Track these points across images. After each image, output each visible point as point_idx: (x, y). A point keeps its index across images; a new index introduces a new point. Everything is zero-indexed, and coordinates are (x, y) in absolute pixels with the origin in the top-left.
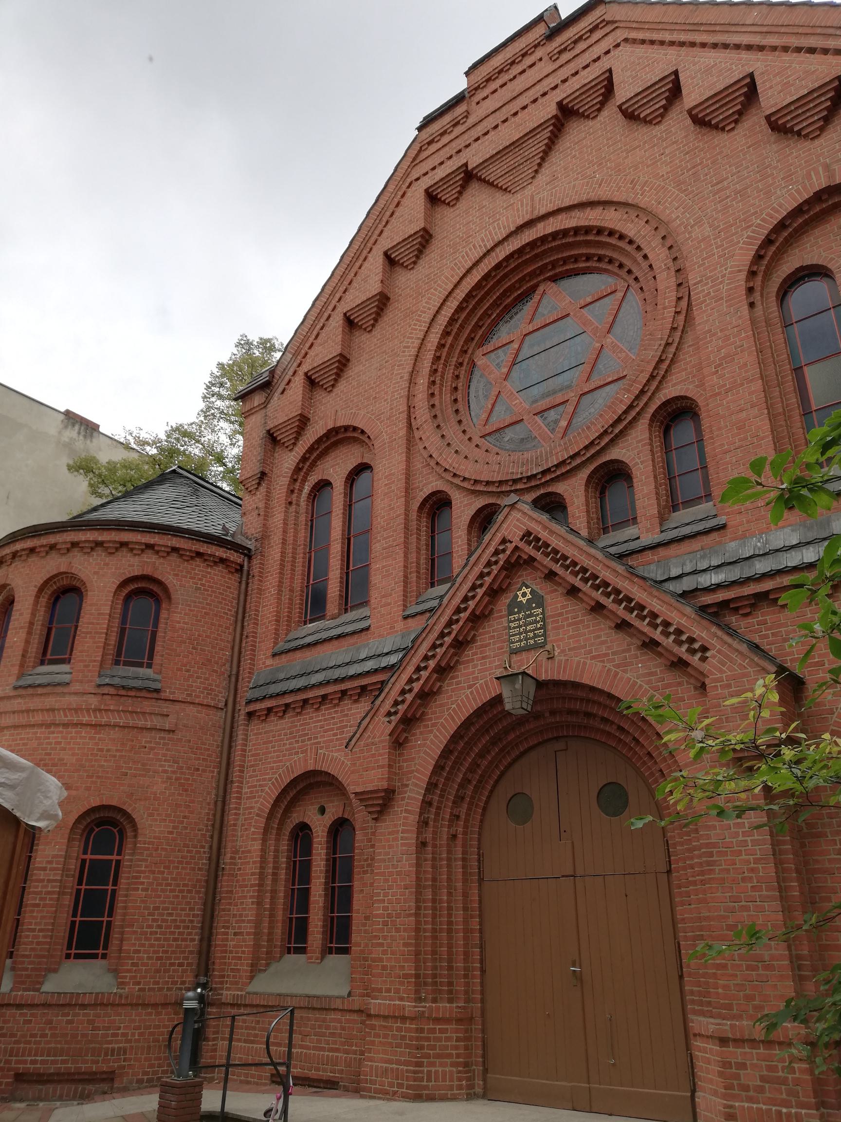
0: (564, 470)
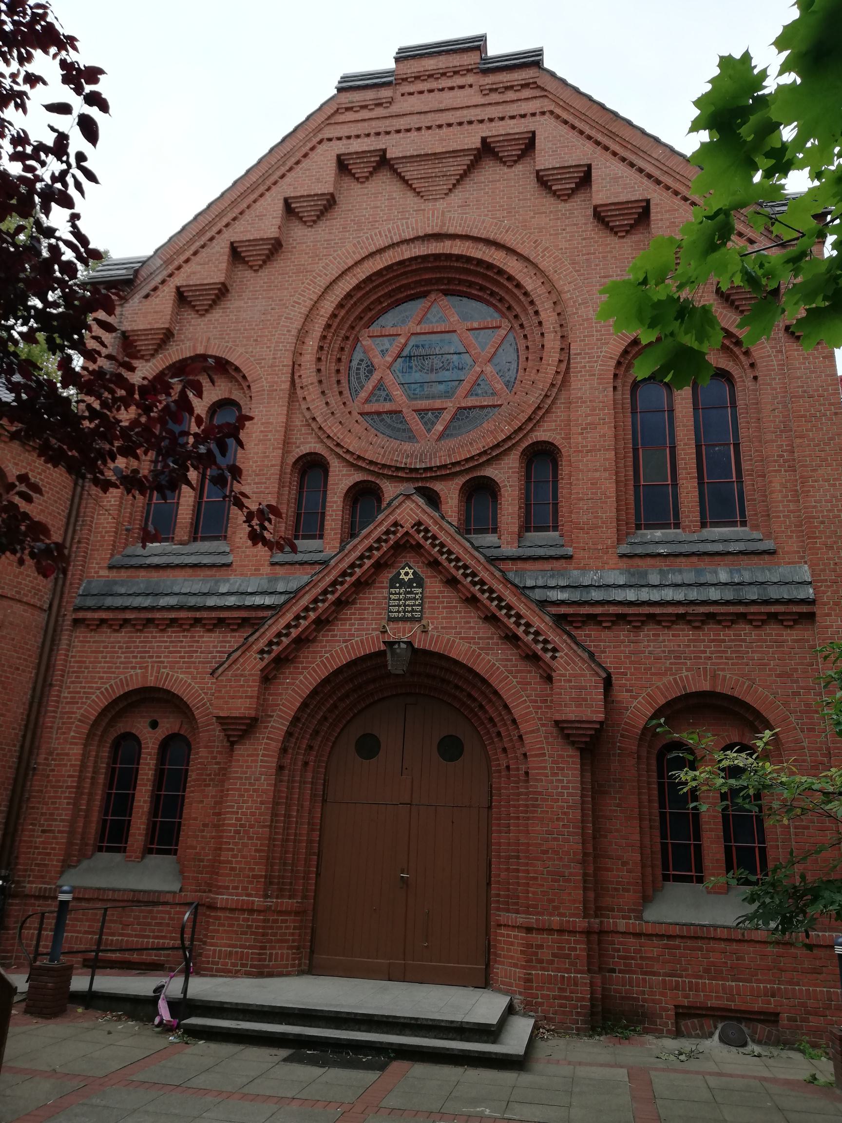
0: (445, 472)
